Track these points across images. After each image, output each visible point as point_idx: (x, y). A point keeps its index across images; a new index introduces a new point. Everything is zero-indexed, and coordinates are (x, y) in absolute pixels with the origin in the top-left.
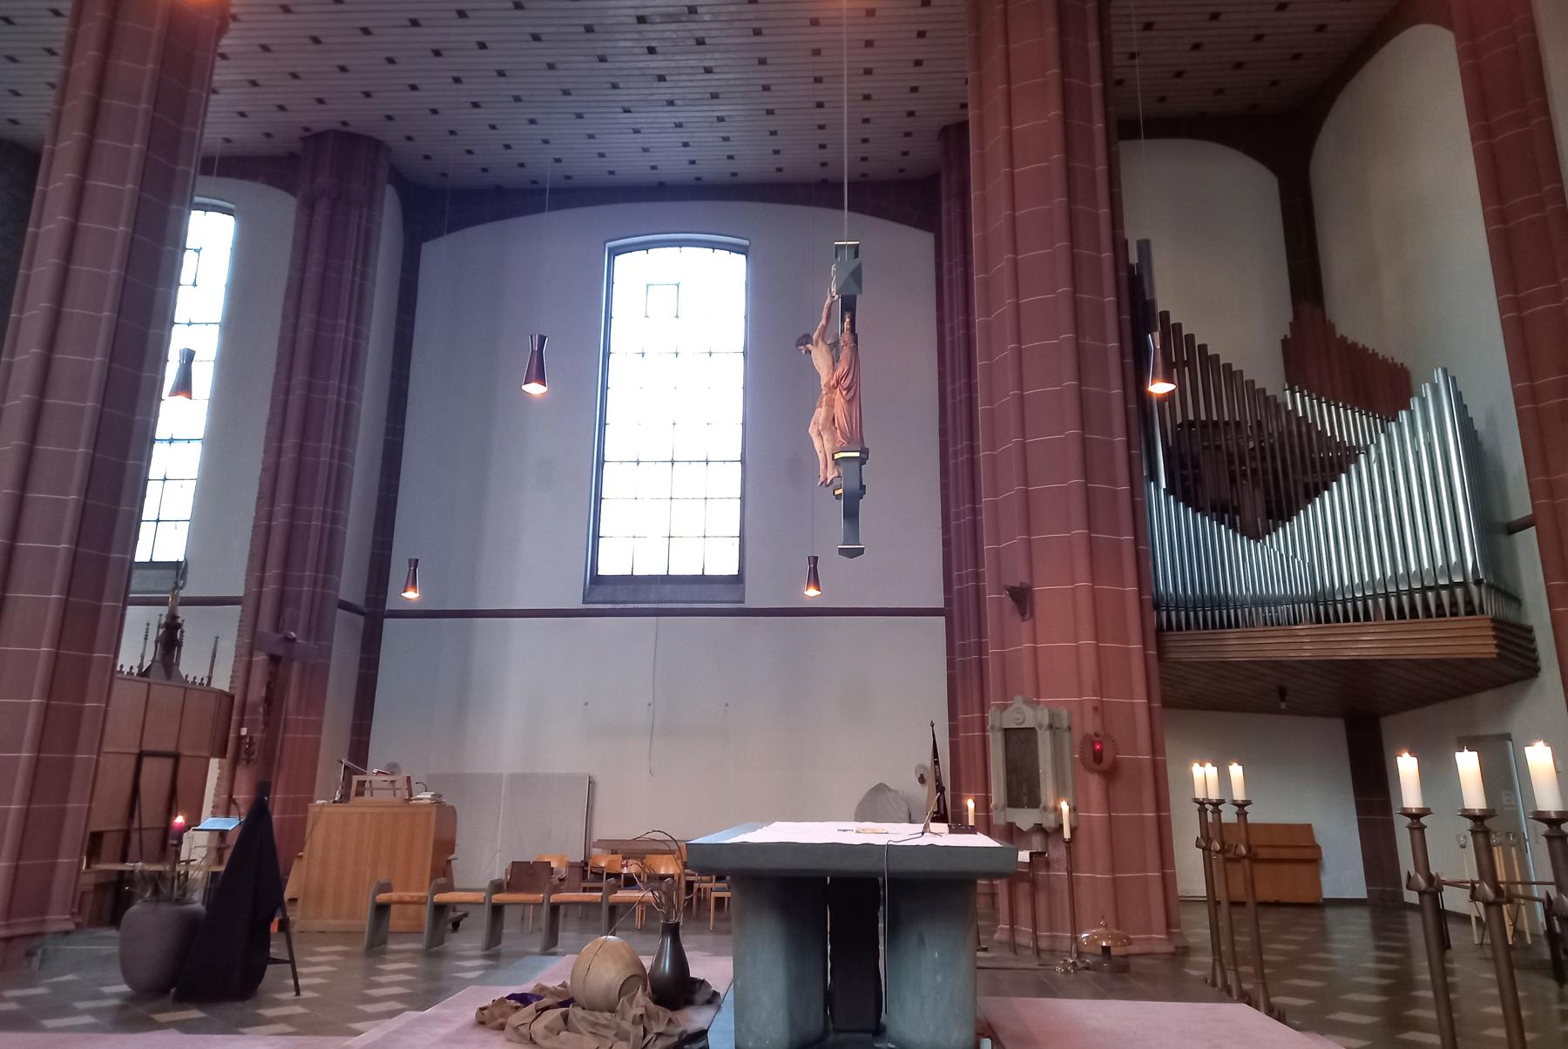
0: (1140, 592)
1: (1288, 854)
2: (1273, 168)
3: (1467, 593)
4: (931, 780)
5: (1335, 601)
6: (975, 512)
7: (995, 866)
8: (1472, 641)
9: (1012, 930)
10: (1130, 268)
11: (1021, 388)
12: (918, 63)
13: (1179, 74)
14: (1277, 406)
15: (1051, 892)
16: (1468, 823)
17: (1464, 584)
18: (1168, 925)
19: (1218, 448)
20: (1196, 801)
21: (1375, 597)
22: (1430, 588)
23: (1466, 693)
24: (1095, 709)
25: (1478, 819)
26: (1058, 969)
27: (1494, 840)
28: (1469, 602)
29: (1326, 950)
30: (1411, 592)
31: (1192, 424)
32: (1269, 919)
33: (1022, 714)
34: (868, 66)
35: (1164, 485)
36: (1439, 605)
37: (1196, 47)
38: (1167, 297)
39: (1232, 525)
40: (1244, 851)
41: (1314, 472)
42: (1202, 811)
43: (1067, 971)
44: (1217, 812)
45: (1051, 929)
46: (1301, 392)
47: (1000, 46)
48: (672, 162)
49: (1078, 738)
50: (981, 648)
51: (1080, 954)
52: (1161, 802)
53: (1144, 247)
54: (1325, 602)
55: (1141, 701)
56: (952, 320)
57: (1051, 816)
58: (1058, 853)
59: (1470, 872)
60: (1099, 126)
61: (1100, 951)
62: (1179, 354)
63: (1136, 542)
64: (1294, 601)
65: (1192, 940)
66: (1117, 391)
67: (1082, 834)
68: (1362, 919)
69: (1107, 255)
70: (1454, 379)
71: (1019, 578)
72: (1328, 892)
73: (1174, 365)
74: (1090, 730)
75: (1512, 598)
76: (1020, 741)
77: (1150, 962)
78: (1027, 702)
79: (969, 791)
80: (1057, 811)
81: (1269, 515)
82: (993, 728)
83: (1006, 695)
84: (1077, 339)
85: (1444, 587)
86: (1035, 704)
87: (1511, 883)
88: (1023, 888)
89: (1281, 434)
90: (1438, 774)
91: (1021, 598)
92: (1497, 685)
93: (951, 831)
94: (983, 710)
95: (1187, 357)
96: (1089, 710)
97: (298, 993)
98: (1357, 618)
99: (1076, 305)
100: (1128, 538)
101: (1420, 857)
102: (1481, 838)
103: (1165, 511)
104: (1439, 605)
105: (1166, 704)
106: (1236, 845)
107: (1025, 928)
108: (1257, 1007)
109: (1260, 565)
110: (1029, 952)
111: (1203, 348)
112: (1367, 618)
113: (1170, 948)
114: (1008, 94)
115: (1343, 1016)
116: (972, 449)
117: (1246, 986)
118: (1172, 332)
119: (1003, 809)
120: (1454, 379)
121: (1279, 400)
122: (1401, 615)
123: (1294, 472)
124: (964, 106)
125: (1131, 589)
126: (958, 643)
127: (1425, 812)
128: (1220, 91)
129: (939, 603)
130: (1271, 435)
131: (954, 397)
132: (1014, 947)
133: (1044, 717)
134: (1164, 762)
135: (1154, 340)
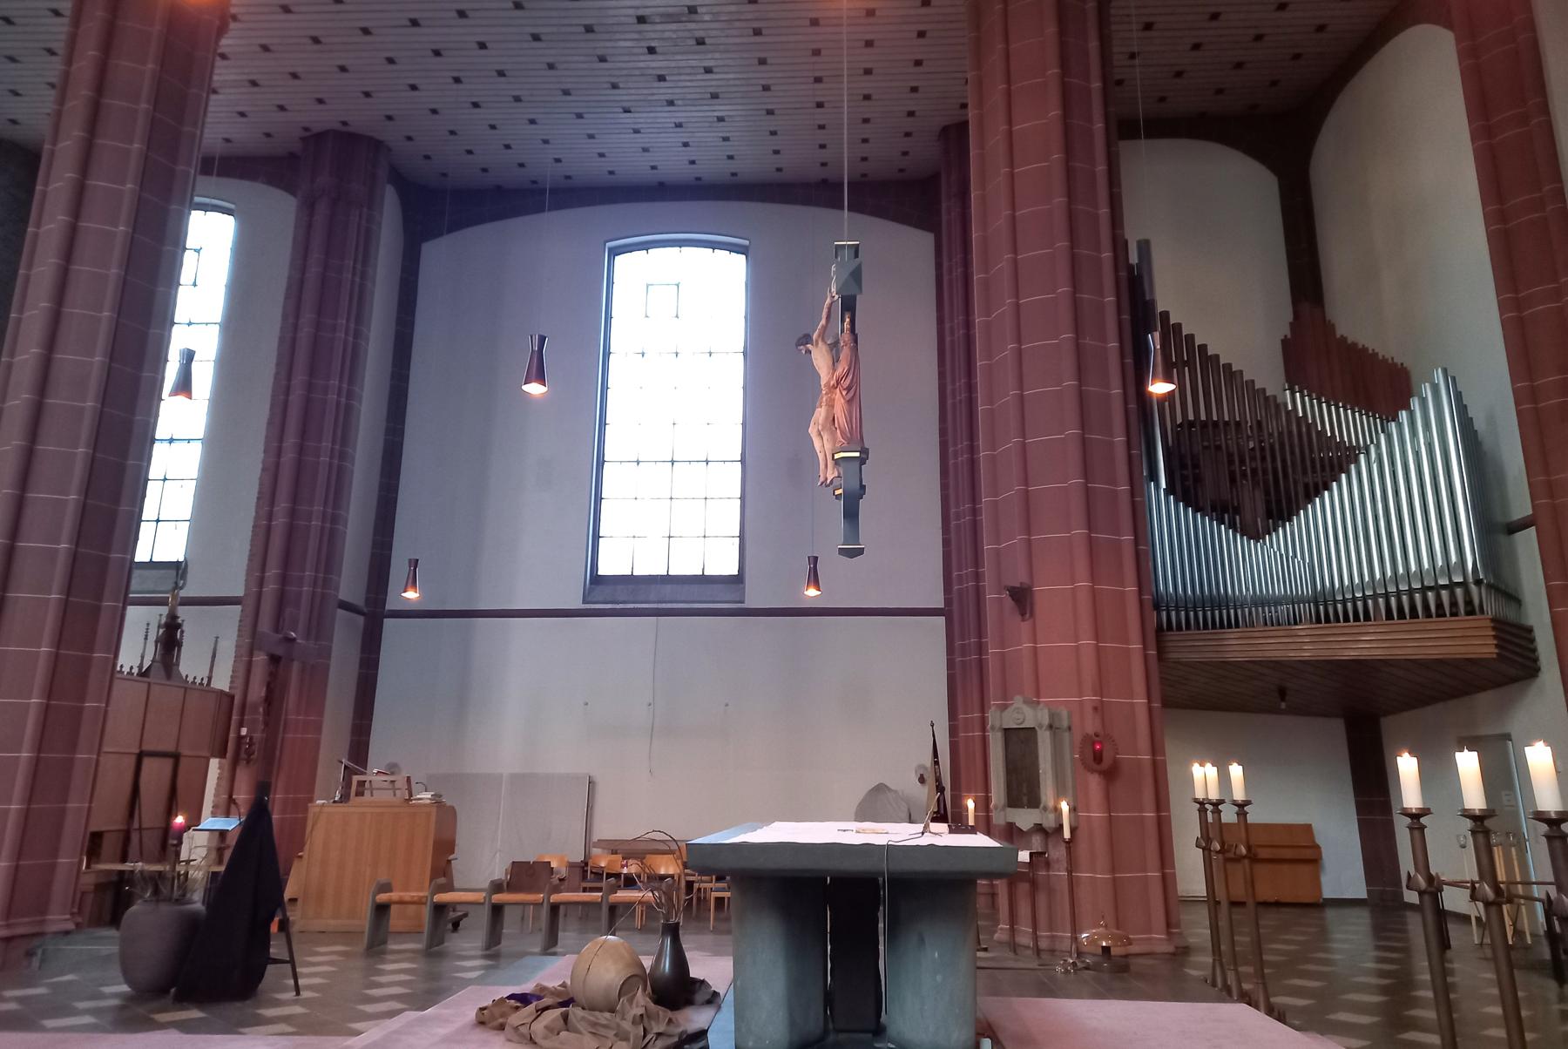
0: (1140, 592)
1: (1288, 854)
2: (1273, 168)
3: (1467, 593)
4: (931, 780)
5: (1335, 601)
6: (975, 512)
7: (995, 866)
8: (1472, 641)
9: (1012, 930)
10: (1130, 268)
11: (1021, 388)
12: (918, 63)
13: (1179, 74)
14: (1277, 406)
15: (1051, 892)
16: (1468, 823)
17: (1464, 584)
18: (1168, 925)
19: (1218, 448)
20: (1196, 801)
21: (1375, 597)
22: (1430, 588)
23: (1466, 693)
24: (1095, 709)
25: (1478, 819)
26: (1058, 969)
27: (1494, 840)
28: (1469, 602)
29: (1326, 950)
30: (1411, 592)
31: (1192, 424)
32: (1269, 919)
33: (1022, 714)
34: (868, 66)
35: (1164, 485)
36: (1439, 605)
37: (1196, 47)
38: (1167, 297)
39: (1232, 525)
40: (1244, 851)
41: (1314, 472)
42: (1202, 811)
43: (1067, 971)
44: (1217, 812)
45: (1051, 929)
46: (1301, 392)
47: (1000, 46)
48: (672, 162)
49: (1078, 738)
50: (981, 648)
51: (1080, 954)
52: (1161, 802)
53: (1144, 247)
54: (1325, 602)
55: (1141, 701)
56: (952, 320)
57: (1051, 816)
58: (1058, 853)
59: (1470, 872)
60: (1099, 126)
61: (1100, 951)
62: (1179, 354)
63: (1136, 542)
64: (1294, 601)
65: (1192, 940)
66: (1117, 391)
67: (1082, 834)
68: (1362, 919)
69: (1107, 255)
70: (1454, 379)
71: (1019, 578)
72: (1328, 892)
73: (1174, 365)
74: (1090, 730)
75: (1512, 598)
76: (1020, 741)
77: (1150, 962)
78: (1027, 702)
79: (969, 791)
80: (1057, 811)
81: (1269, 515)
82: (993, 728)
83: (1006, 695)
84: (1077, 339)
85: (1444, 587)
86: (1035, 704)
87: (1511, 883)
88: (1023, 888)
89: (1281, 434)
90: (1438, 774)
91: (1021, 598)
92: (1497, 685)
93: (951, 831)
94: (983, 710)
95: (1187, 357)
96: (1089, 710)
97: (298, 993)
98: (1357, 618)
99: (1076, 305)
100: (1128, 538)
101: (1420, 857)
102: (1481, 838)
103: (1165, 511)
104: (1439, 605)
105: (1166, 704)
106: (1236, 845)
107: (1025, 928)
108: (1257, 1007)
109: (1260, 565)
110: (1029, 952)
111: (1203, 348)
112: (1367, 618)
113: (1170, 948)
114: (1008, 94)
115: (1343, 1016)
116: (972, 449)
117: (1246, 986)
118: (1172, 332)
119: (1003, 809)
120: (1454, 379)
121: (1279, 400)
122: (1401, 615)
123: (1294, 472)
124: (964, 106)
125: (1131, 589)
126: (958, 643)
127: (1425, 812)
128: (1220, 91)
129: (939, 603)
130: (1271, 435)
131: (954, 397)
132: (1014, 947)
133: (1044, 717)
134: (1164, 762)
135: (1154, 340)
